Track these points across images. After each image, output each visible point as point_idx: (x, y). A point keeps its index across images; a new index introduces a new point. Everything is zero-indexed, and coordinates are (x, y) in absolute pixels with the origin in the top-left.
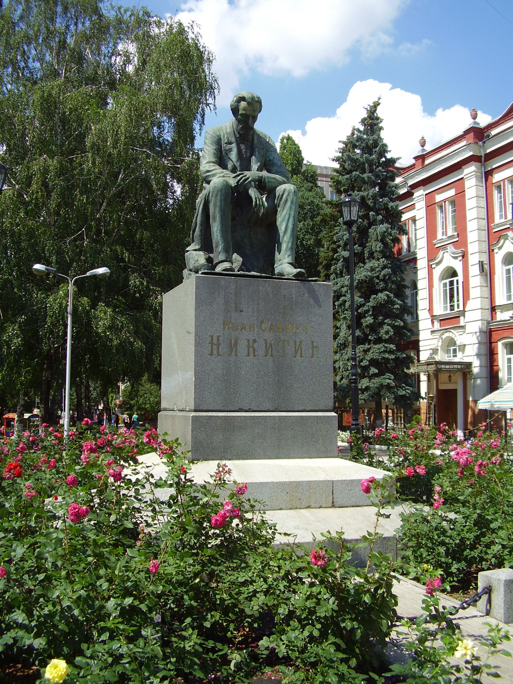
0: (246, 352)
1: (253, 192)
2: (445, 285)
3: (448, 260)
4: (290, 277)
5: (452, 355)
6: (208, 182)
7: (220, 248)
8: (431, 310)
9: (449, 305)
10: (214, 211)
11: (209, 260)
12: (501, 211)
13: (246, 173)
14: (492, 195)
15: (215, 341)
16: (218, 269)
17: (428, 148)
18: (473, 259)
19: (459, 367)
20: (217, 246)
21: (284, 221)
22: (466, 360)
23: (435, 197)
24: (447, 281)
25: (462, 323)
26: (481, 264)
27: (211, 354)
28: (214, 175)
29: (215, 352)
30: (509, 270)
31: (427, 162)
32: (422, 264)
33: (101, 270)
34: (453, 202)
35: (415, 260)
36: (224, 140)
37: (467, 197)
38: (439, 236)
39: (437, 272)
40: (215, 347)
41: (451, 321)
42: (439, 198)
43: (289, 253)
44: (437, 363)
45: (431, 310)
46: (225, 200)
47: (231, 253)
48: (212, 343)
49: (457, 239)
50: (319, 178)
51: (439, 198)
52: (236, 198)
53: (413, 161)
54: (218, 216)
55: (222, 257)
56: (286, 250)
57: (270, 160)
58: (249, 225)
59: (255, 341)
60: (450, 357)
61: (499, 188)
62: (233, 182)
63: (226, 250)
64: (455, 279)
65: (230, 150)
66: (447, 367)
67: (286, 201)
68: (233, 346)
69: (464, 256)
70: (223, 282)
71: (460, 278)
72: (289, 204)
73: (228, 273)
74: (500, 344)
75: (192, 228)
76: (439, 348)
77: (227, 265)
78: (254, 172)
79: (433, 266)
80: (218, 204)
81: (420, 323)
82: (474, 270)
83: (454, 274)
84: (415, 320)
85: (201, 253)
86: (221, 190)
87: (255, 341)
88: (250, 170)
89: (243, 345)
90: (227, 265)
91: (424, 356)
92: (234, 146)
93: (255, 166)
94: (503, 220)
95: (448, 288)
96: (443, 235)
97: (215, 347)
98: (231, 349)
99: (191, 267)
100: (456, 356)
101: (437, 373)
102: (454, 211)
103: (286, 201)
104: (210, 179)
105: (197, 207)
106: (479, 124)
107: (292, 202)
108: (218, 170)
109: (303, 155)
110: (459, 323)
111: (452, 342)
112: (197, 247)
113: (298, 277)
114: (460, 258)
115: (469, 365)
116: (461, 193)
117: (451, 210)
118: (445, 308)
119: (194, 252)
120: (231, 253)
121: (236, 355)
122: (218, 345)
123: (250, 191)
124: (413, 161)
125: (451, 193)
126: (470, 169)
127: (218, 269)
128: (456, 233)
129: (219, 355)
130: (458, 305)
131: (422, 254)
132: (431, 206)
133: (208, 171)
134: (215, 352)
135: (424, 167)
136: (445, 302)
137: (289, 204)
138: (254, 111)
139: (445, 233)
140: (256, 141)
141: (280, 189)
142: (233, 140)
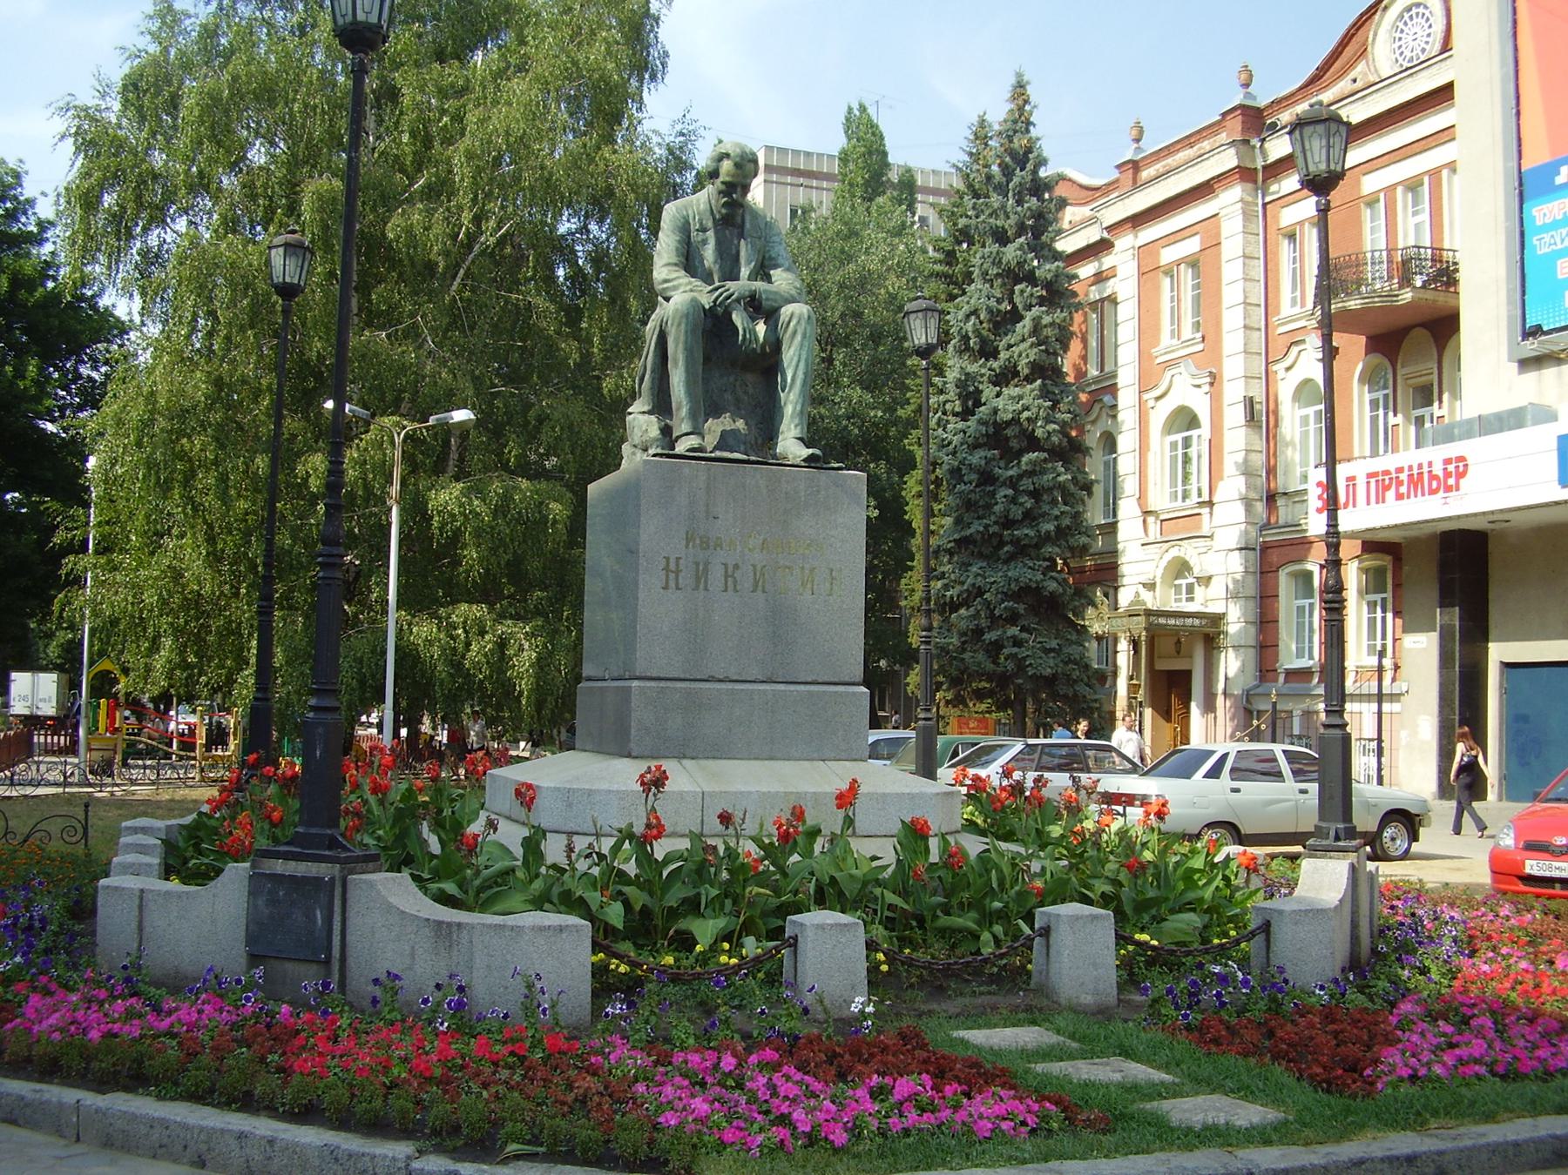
0: (722, 585)
1: (738, 318)
2: (1174, 445)
3: (1186, 391)
4: (798, 461)
5: (1184, 596)
6: (667, 299)
7: (684, 411)
8: (1142, 497)
9: (1180, 488)
10: (676, 349)
11: (666, 431)
12: (1294, 289)
13: (729, 284)
14: (1276, 254)
15: (672, 566)
16: (681, 448)
17: (1151, 145)
18: (1234, 392)
19: (1197, 622)
20: (679, 409)
21: (795, 360)
22: (1216, 608)
23: (1158, 254)
24: (1179, 437)
25: (1205, 531)
26: (1250, 403)
27: (665, 588)
28: (675, 288)
29: (672, 584)
30: (1307, 416)
31: (1145, 174)
32: (1126, 398)
33: (461, 415)
34: (1193, 262)
35: (1113, 389)
36: (694, 226)
37: (1225, 257)
38: (1166, 340)
39: (1160, 414)
40: (672, 576)
41: (1182, 526)
42: (1168, 255)
43: (797, 421)
44: (1149, 613)
45: (1142, 497)
46: (693, 331)
47: (701, 420)
48: (666, 569)
49: (1200, 347)
50: (919, 197)
51: (1168, 255)
52: (713, 327)
53: (1115, 175)
54: (681, 363)
55: (685, 427)
56: (792, 417)
57: (771, 258)
58: (733, 363)
59: (736, 567)
60: (1180, 600)
61: (1291, 237)
62: (707, 301)
63: (693, 415)
64: (1194, 433)
65: (705, 242)
66: (1172, 622)
67: (795, 333)
68: (701, 576)
69: (1214, 379)
70: (686, 471)
71: (1205, 431)
72: (799, 337)
73: (695, 455)
74: (1283, 576)
75: (639, 374)
76: (1158, 580)
77: (693, 441)
78: (743, 284)
79: (1151, 403)
80: (682, 338)
81: (28, 675)
82: (1235, 415)
83: (1192, 421)
84: (1111, 520)
85: (653, 418)
86: (687, 315)
87: (736, 567)
88: (737, 279)
89: (717, 574)
90: (693, 441)
91: (1125, 598)
92: (710, 234)
93: (745, 272)
94: (1297, 310)
95: (1180, 452)
96: (1172, 337)
97: (672, 576)
98: (698, 579)
99: (636, 442)
100: (1192, 599)
101: (1154, 634)
102: (1196, 287)
103: (795, 333)
104: (669, 294)
105: (648, 338)
106: (1254, 98)
107: (804, 336)
108: (683, 279)
109: (889, 144)
110: (1199, 527)
111: (1181, 568)
112: (646, 408)
113: (811, 461)
114: (1206, 388)
115: (1217, 619)
116: (1213, 246)
117: (1190, 283)
118: (1174, 496)
119: (640, 417)
120: (701, 420)
121: (706, 589)
122: (677, 572)
123: (734, 316)
124: (1115, 175)
125: (1192, 246)
126: (1231, 198)
127: (681, 448)
128: (1199, 335)
129: (678, 588)
130: (1199, 490)
131: (1127, 377)
132: (1148, 272)
133: (666, 281)
134: (672, 584)
135: (1137, 186)
136: (1173, 483)
137: (799, 337)
138: (745, 177)
139: (1176, 333)
140: (748, 225)
141: (786, 311)
142: (710, 224)
